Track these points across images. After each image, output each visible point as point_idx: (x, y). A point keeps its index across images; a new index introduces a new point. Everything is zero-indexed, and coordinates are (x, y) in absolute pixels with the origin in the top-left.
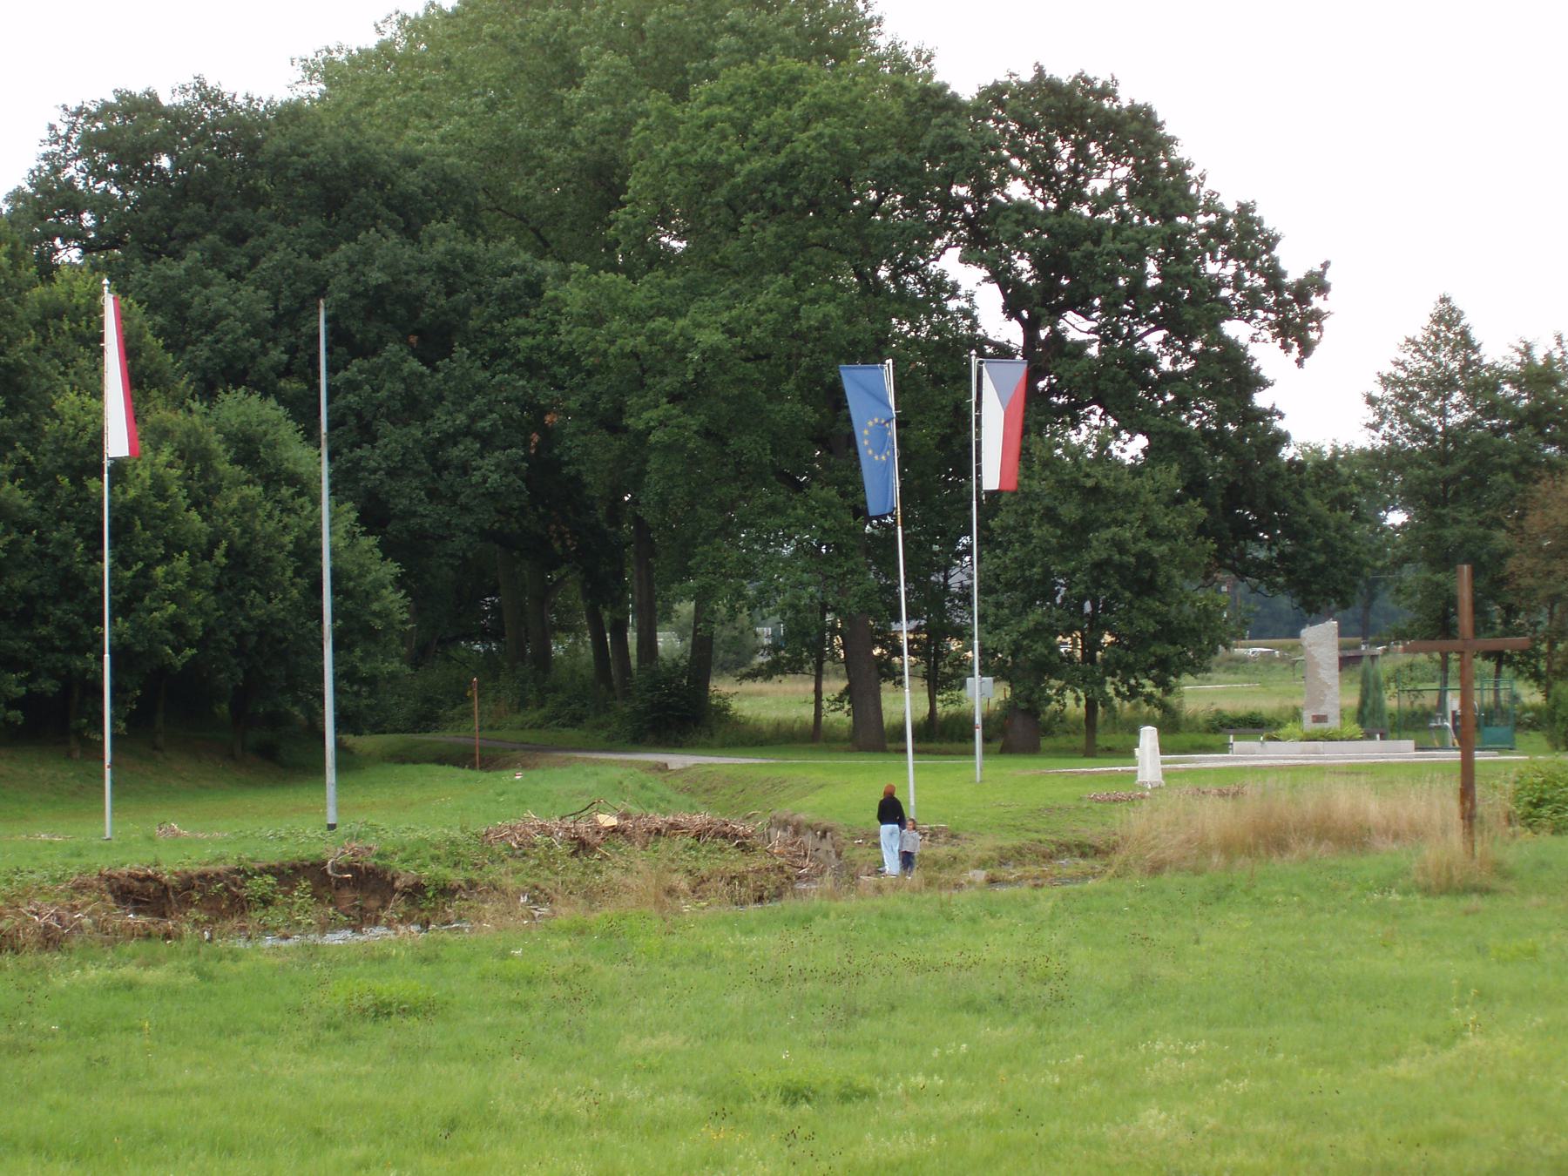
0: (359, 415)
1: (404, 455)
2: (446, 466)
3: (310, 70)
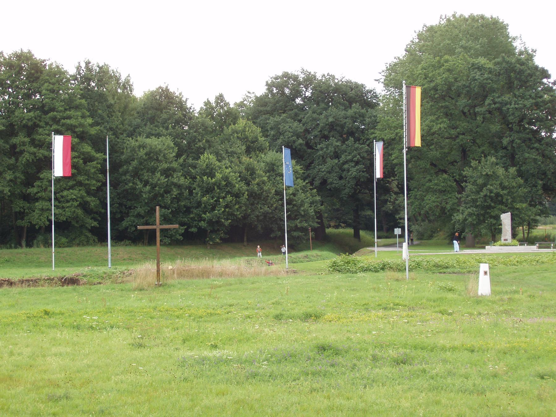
0: (323, 157)
1: (332, 167)
2: (344, 170)
3: (303, 71)
